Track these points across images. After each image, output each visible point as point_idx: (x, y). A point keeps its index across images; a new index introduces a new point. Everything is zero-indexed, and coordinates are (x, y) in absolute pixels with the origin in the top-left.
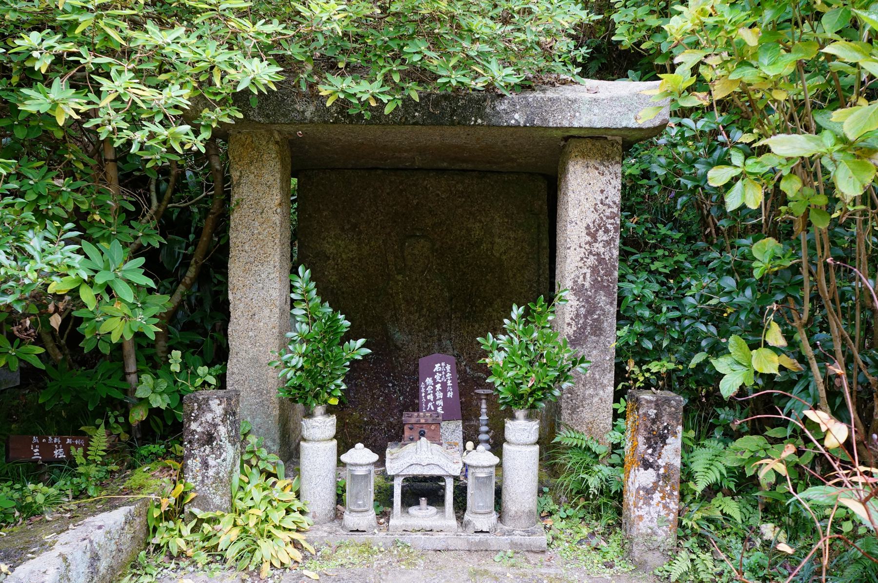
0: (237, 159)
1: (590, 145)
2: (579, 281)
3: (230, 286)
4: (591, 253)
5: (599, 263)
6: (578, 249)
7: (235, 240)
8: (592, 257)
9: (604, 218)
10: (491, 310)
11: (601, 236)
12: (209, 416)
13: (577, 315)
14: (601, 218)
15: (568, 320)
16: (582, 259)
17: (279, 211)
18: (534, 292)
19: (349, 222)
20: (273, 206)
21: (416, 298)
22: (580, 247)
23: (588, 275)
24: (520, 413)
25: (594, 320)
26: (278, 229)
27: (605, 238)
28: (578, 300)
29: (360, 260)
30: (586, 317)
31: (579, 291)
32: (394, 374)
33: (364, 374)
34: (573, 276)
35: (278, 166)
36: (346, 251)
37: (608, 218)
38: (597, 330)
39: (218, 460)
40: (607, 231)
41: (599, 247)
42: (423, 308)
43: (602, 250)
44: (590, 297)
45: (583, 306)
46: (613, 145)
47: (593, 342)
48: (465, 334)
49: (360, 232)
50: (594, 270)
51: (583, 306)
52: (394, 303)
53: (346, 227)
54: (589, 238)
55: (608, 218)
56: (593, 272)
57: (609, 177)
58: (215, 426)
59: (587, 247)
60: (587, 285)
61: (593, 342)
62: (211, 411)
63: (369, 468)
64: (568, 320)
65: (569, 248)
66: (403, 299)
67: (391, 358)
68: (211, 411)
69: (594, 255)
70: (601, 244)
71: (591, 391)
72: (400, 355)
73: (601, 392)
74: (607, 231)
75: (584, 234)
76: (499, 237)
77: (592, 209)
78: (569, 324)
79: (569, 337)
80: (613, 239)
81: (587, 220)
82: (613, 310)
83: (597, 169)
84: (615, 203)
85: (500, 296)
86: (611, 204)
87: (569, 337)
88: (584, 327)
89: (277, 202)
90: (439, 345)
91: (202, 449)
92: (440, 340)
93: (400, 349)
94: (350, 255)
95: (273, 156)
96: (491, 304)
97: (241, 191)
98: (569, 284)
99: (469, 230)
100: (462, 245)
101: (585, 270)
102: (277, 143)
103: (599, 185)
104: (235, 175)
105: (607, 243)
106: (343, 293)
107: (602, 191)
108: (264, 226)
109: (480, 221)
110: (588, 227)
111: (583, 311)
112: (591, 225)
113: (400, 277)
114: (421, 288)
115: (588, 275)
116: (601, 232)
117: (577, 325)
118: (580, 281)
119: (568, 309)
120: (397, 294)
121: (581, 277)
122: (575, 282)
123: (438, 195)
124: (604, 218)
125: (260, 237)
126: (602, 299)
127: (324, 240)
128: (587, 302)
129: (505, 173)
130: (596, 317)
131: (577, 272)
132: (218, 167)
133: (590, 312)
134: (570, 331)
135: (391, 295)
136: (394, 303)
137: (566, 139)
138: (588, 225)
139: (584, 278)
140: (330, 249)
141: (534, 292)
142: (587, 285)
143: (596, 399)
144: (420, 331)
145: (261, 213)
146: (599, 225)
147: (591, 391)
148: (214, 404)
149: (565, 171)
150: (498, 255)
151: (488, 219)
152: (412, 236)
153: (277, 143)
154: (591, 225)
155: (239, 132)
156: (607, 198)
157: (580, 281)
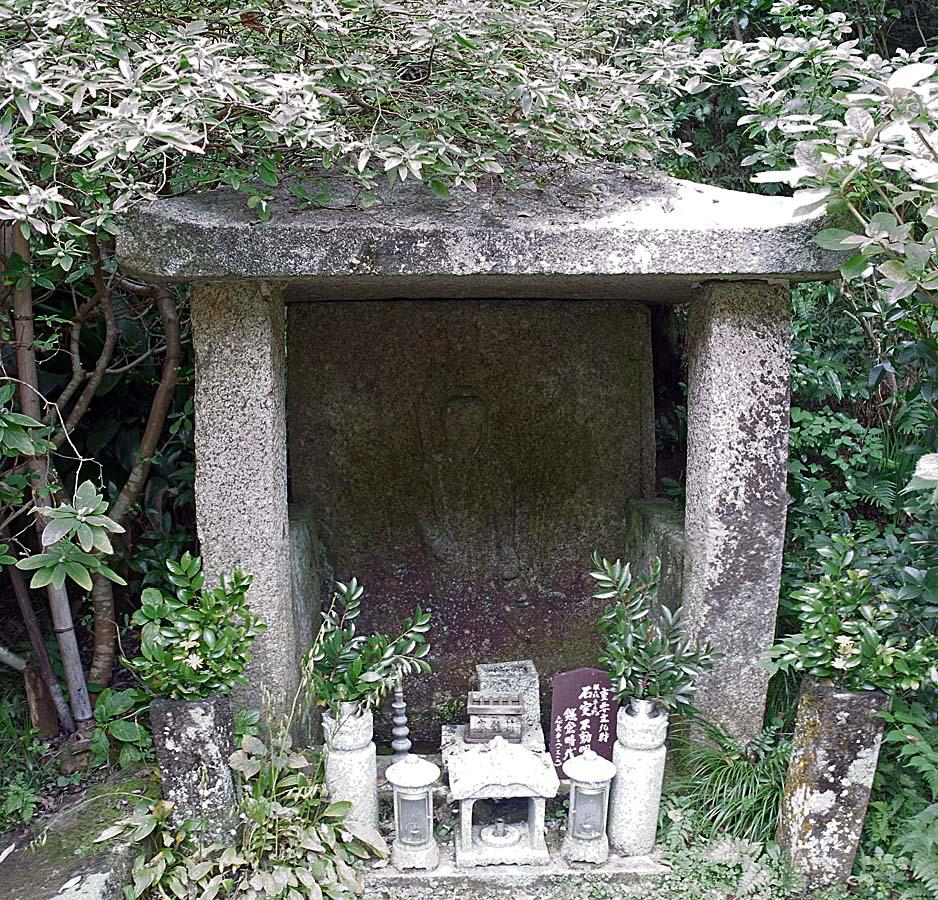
0: (204, 326)
1: (742, 293)
2: (728, 499)
3: (200, 519)
4: (746, 457)
5: (758, 471)
6: (727, 452)
7: (203, 449)
8: (748, 463)
9: (767, 403)
10: (572, 501)
11: (762, 430)
12: (191, 731)
13: (726, 551)
14: (762, 404)
15: (711, 559)
16: (733, 466)
17: (269, 403)
18: (635, 474)
19: (363, 378)
20: (260, 397)
21: (465, 488)
22: (731, 448)
23: (742, 490)
24: (643, 707)
25: (750, 558)
26: (268, 431)
27: (767, 434)
28: (727, 528)
29: (381, 433)
30: (738, 553)
31: (727, 512)
32: (434, 594)
33: (391, 596)
34: (718, 491)
35: (268, 334)
36: (360, 419)
37: (772, 402)
38: (755, 574)
39: (212, 790)
40: (770, 423)
41: (759, 448)
42: (474, 502)
43: (763, 452)
44: (745, 523)
45: (735, 538)
46: (776, 290)
47: (747, 589)
48: (535, 537)
49: (380, 393)
50: (751, 482)
51: (735, 538)
52: (432, 496)
53: (360, 386)
54: (743, 435)
55: (772, 402)
56: (749, 485)
57: (773, 341)
58: (203, 743)
59: (741, 448)
60: (740, 504)
61: (747, 589)
62: (193, 724)
63: (426, 789)
64: (711, 559)
65: (713, 451)
66: (445, 487)
67: (429, 572)
68: (193, 724)
69: (751, 460)
70: (762, 444)
71: (740, 659)
72: (442, 570)
73: (754, 661)
74: (770, 423)
75: (736, 428)
76: (584, 396)
77: (749, 391)
78: (712, 564)
79: (712, 583)
80: (780, 435)
81: (741, 407)
82: (778, 542)
83: (754, 329)
84: (781, 379)
85: (585, 481)
86: (777, 381)
87: (712, 583)
88: (734, 567)
89: (267, 390)
90: (498, 554)
91: (188, 776)
92: (499, 547)
93: (443, 562)
94: (366, 426)
95: (260, 319)
96: (573, 492)
97: (211, 374)
98: (713, 503)
99: (539, 387)
100: (529, 408)
101: (737, 483)
102: (265, 299)
103: (757, 353)
104: (200, 349)
105: (771, 441)
106: (357, 481)
107: (763, 363)
108: (248, 427)
109: (556, 374)
110: (742, 418)
111: (734, 544)
112: (747, 415)
113: (438, 458)
114: (471, 472)
115: (742, 490)
116: (761, 425)
117: (724, 565)
118: (729, 499)
119: (710, 543)
120: (435, 481)
121: (731, 494)
122: (722, 501)
123: (493, 336)
124: (767, 403)
125: (241, 444)
126: (762, 528)
127: (326, 405)
128: (741, 531)
129: (590, 301)
130: (753, 552)
131: (724, 486)
132: (171, 316)
133: (743, 547)
134: (714, 574)
135: (428, 483)
136: (432, 496)
137: (706, 283)
138: (743, 415)
139: (736, 494)
140: (334, 416)
141: (635, 474)
142: (740, 504)
143: (745, 670)
144: (471, 535)
145: (243, 408)
146: (758, 414)
147: (740, 659)
148: (196, 713)
149: (703, 332)
150: (582, 422)
151: (567, 371)
152: (456, 397)
153: (265, 299)
154: (747, 415)
155: (208, 285)
156: (769, 372)
157: (729, 499)
